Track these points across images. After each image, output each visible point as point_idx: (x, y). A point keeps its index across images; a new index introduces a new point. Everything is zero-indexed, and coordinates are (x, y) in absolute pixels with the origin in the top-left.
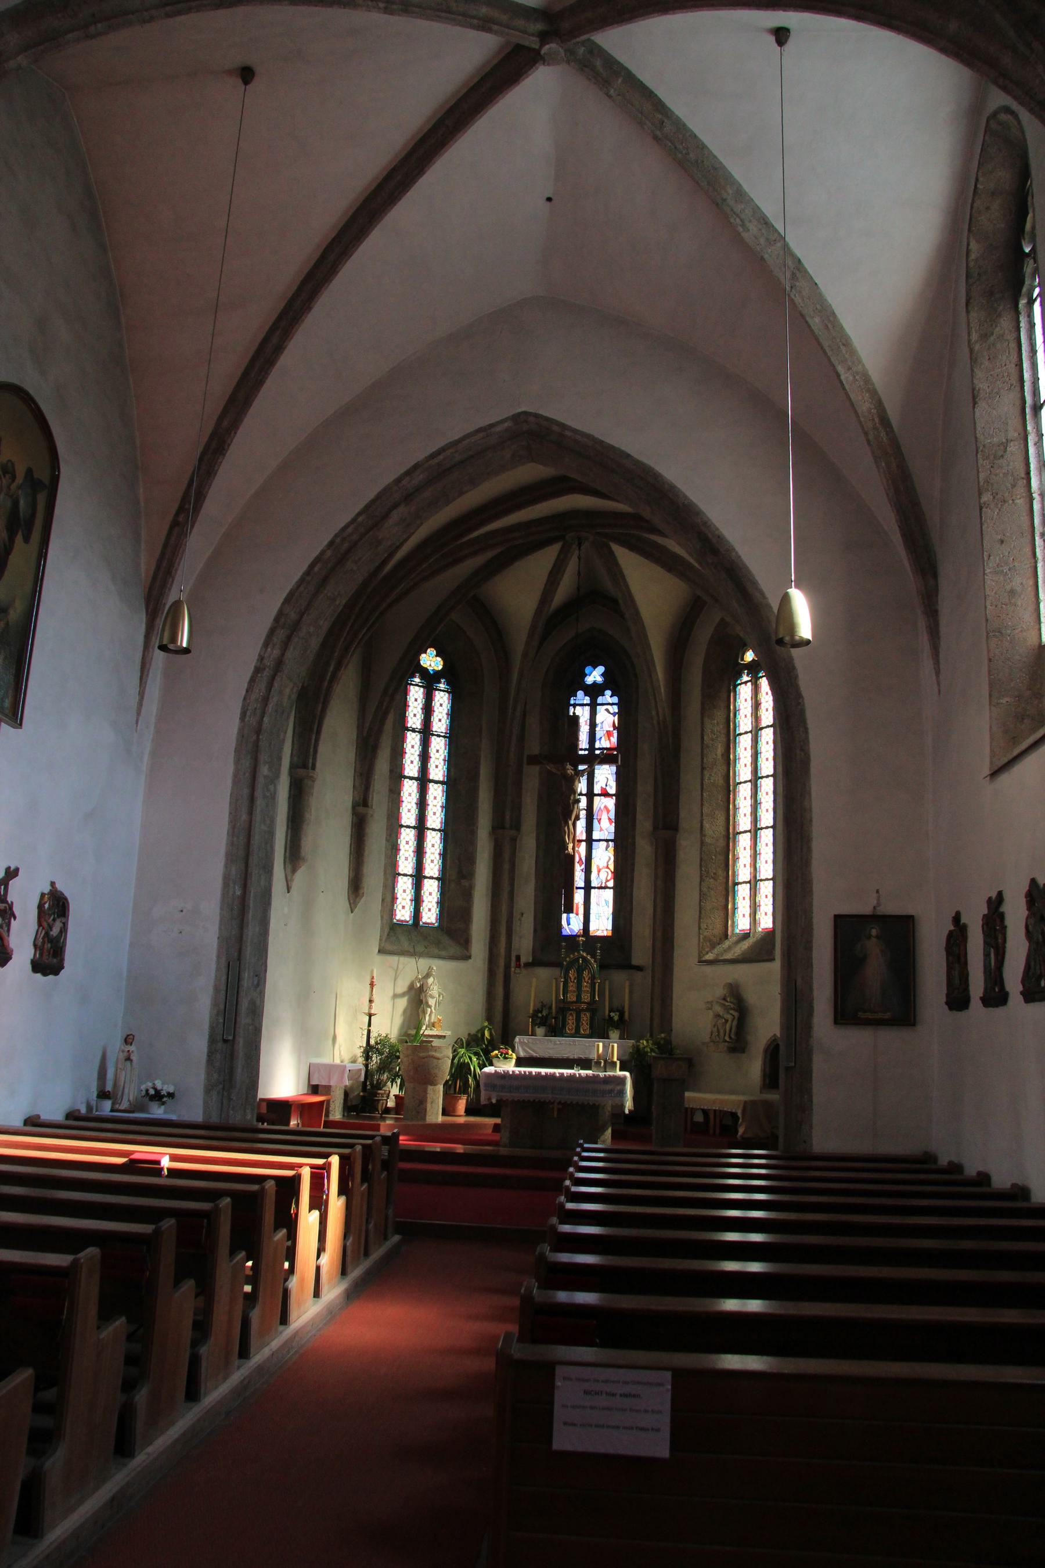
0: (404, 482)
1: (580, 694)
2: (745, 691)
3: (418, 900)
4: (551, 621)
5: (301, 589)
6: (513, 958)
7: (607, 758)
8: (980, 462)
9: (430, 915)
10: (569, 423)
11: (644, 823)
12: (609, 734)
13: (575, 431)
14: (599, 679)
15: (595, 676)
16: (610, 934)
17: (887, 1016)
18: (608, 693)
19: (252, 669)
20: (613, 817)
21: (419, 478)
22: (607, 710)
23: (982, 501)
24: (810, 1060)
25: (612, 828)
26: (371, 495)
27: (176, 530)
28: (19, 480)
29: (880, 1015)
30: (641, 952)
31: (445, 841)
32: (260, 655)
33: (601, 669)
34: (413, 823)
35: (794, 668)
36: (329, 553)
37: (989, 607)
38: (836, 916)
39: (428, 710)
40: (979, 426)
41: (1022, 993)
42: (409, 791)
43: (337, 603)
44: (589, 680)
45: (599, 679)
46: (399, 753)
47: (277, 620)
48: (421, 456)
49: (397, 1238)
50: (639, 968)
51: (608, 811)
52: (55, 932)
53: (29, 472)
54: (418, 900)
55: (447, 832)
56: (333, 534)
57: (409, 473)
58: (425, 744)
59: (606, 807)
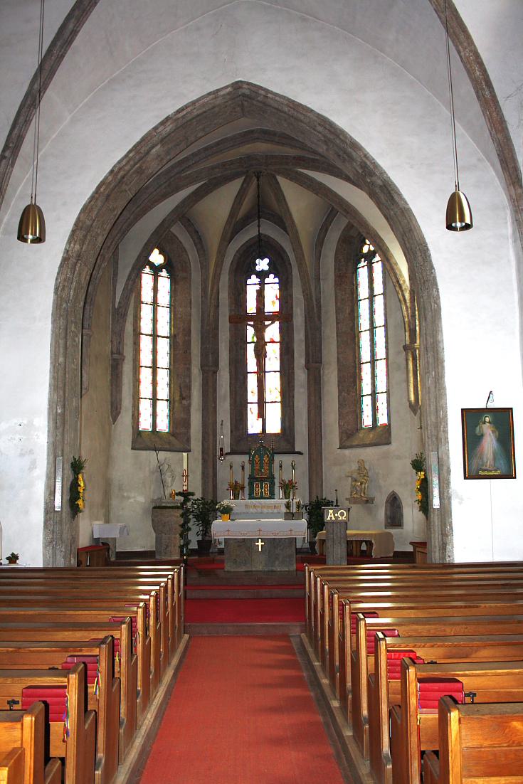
1: (254, 277)
2: (363, 273)
4: (235, 226)
5: (92, 203)
6: (218, 450)
7: (273, 317)
9: (163, 425)
10: (271, 89)
11: (300, 360)
13: (276, 94)
14: (266, 268)
15: (263, 265)
17: (498, 473)
18: (272, 276)
21: (169, 127)
26: (138, 139)
30: (301, 443)
32: (65, 249)
33: (266, 261)
35: (428, 249)
36: (110, 178)
38: (462, 410)
42: (146, 343)
43: (115, 213)
44: (258, 268)
45: (266, 268)
46: (137, 318)
47: (76, 224)
48: (170, 111)
49: (187, 636)
50: (300, 453)
55: (172, 370)
56: (113, 165)
57: (162, 123)
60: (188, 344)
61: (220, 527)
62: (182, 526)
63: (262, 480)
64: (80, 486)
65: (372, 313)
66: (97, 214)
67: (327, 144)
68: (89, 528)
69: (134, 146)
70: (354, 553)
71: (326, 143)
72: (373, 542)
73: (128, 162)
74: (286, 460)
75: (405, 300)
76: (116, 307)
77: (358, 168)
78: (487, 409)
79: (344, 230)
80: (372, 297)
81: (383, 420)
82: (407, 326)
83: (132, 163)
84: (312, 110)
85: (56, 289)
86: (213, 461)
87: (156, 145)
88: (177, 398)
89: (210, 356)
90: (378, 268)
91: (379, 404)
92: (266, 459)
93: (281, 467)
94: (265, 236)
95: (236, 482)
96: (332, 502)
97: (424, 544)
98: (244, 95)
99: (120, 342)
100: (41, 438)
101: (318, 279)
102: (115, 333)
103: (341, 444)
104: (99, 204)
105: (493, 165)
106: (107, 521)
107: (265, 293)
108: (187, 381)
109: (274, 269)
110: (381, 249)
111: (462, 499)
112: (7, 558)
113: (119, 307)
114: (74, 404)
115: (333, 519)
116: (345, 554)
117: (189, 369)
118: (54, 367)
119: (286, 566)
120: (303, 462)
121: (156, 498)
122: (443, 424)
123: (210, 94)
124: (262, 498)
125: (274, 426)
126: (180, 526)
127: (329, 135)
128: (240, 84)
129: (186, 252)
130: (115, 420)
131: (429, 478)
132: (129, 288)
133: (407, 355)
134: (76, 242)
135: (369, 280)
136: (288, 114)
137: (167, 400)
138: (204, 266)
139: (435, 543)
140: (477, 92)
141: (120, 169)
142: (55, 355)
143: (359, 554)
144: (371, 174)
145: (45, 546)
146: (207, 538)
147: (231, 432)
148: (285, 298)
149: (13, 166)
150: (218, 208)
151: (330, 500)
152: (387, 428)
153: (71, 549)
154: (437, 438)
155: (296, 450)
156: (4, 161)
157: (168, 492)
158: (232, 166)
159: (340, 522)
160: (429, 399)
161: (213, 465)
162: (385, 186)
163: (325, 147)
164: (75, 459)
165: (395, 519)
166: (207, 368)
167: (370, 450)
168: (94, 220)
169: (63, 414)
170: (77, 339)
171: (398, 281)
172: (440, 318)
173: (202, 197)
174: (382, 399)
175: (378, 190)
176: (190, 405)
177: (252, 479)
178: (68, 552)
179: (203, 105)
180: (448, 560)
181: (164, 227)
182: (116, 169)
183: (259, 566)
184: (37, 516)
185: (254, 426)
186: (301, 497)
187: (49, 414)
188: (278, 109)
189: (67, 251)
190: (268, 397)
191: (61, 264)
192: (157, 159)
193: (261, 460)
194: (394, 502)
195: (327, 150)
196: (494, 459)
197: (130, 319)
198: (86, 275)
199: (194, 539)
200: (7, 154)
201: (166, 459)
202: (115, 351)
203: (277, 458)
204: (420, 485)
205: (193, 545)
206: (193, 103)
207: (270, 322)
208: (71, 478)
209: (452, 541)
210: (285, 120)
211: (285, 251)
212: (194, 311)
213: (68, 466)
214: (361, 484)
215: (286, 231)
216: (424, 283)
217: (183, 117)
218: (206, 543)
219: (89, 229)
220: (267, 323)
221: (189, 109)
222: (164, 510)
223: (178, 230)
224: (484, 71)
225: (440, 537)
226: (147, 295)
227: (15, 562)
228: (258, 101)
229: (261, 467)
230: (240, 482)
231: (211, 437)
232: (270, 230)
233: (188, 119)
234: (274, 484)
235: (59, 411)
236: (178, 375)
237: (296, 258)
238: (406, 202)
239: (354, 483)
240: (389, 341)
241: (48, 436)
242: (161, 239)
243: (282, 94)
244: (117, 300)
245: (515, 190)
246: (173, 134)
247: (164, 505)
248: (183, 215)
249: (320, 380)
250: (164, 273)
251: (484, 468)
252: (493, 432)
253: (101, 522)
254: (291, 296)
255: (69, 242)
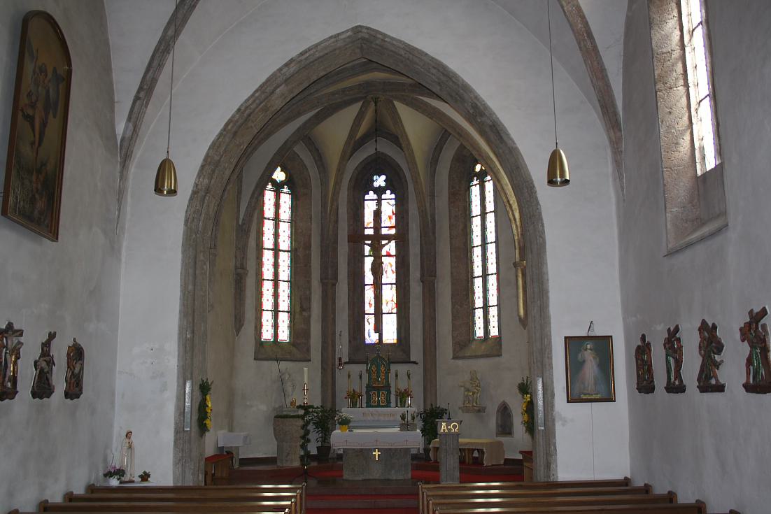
0: (284, 70)
1: (371, 193)
2: (475, 191)
3: (276, 326)
4: (355, 144)
5: (220, 140)
6: (337, 360)
8: (655, 63)
9: (284, 335)
12: (390, 218)
14: (383, 184)
15: (380, 181)
16: (395, 342)
18: (388, 192)
19: (190, 192)
20: (394, 268)
21: (293, 68)
22: (388, 203)
23: (657, 87)
24: (554, 425)
25: (394, 276)
26: (263, 79)
27: (138, 102)
28: (50, 76)
29: (593, 397)
30: (416, 353)
31: (291, 288)
32: (195, 183)
33: (383, 177)
34: (281, 283)
35: (534, 186)
37: (663, 153)
38: (566, 338)
39: (277, 206)
40: (654, 43)
41: (698, 387)
44: (376, 184)
45: (383, 184)
46: (260, 234)
47: (205, 160)
48: (294, 54)
50: (415, 363)
51: (391, 266)
52: (77, 371)
53: (55, 70)
54: (276, 326)
55: (293, 282)
56: (239, 104)
57: (287, 65)
58: (277, 227)
59: (390, 263)
60: (308, 258)
61: (340, 438)
62: (303, 437)
63: (378, 389)
64: (208, 406)
65: (484, 229)
66: (225, 149)
67: (440, 85)
68: (217, 438)
69: (260, 86)
70: (467, 460)
71: (439, 84)
72: (484, 450)
73: (254, 101)
74: (402, 369)
75: (515, 220)
76: (240, 223)
77: (469, 108)
78: (588, 337)
79: (458, 149)
80: (485, 276)
81: (494, 332)
82: (517, 244)
83: (257, 101)
84: (427, 54)
85: (186, 222)
86: (332, 369)
87: (281, 85)
88: (298, 310)
89: (330, 269)
90: (489, 186)
91: (489, 254)
92: (382, 369)
93: (397, 376)
94: (382, 153)
95: (354, 390)
96: (446, 410)
97: (530, 453)
98: (363, 39)
99: (243, 258)
100: (172, 362)
101: (432, 195)
102: (239, 249)
103: (454, 354)
104: (227, 140)
105: (594, 107)
106: (231, 430)
107: (380, 209)
108: (308, 293)
109: (390, 185)
110: (493, 171)
111: (566, 421)
112: (140, 476)
113: (243, 224)
114: (202, 328)
115: (446, 431)
116: (457, 465)
117: (309, 282)
118: (184, 294)
119: (402, 474)
120: (417, 372)
121: (277, 406)
122: (547, 350)
123: (331, 37)
124: (378, 406)
125: (390, 335)
126: (301, 437)
127: (442, 77)
128: (360, 29)
129: (307, 169)
130: (238, 331)
131: (535, 401)
132: (252, 205)
133: (517, 271)
134: (204, 176)
135: (482, 197)
136: (404, 57)
137: (288, 312)
138: (324, 182)
139: (540, 462)
140: (579, 44)
141: (247, 108)
142: (185, 284)
143: (471, 462)
144: (482, 114)
145: (175, 464)
146: (326, 445)
147: (350, 341)
148: (401, 214)
149: (146, 107)
150: (337, 130)
151: (444, 408)
152: (498, 339)
153: (199, 466)
154: (542, 364)
155: (412, 360)
156: (138, 101)
157: (289, 400)
158: (351, 92)
159: (453, 434)
160: (535, 327)
161: (332, 373)
162: (494, 126)
163: (439, 88)
164: (203, 381)
165: (505, 428)
166: (326, 281)
167: (482, 362)
168: (222, 156)
169: (192, 339)
170: (205, 267)
171: (508, 201)
172: (545, 252)
173: (326, 117)
174: (493, 312)
175: (488, 129)
176: (309, 317)
177: (370, 388)
178: (197, 469)
179: (325, 48)
180: (552, 479)
181: (286, 147)
182: (243, 108)
183: (376, 473)
184: (168, 435)
185: (371, 337)
186: (413, 406)
187: (179, 338)
188: (395, 52)
189: (196, 185)
190: (385, 309)
191: (191, 197)
192: (281, 97)
193: (378, 370)
194: (504, 411)
195: (441, 90)
196: (595, 384)
197: (253, 235)
198: (215, 206)
199: (313, 449)
200: (142, 95)
201: (287, 369)
202: (239, 266)
203: (394, 368)
204: (527, 407)
205: (314, 451)
206: (316, 46)
207: (387, 241)
208: (200, 399)
209: (556, 460)
210: (402, 62)
211: (401, 169)
212: (314, 226)
213: (197, 388)
214: (474, 394)
215: (402, 150)
216: (530, 218)
217: (306, 59)
218: (325, 449)
219: (217, 164)
220: (384, 242)
221: (312, 52)
222: (285, 420)
223: (301, 151)
224: (586, 24)
225: (545, 456)
226: (269, 211)
227: (147, 480)
228: (377, 44)
229: (378, 376)
230: (358, 390)
231: (330, 348)
232: (385, 147)
233: (311, 60)
234: (390, 393)
235: (188, 336)
236: (298, 288)
237: (412, 176)
238: (513, 142)
239: (466, 393)
240: (500, 259)
241: (178, 360)
242: (282, 159)
243: (398, 38)
244: (241, 217)
245: (615, 133)
246: (296, 75)
247: (285, 413)
248: (306, 137)
249: (434, 293)
250: (286, 189)
251: (585, 392)
252: (594, 358)
253: (224, 431)
254: (407, 212)
255: (199, 176)
